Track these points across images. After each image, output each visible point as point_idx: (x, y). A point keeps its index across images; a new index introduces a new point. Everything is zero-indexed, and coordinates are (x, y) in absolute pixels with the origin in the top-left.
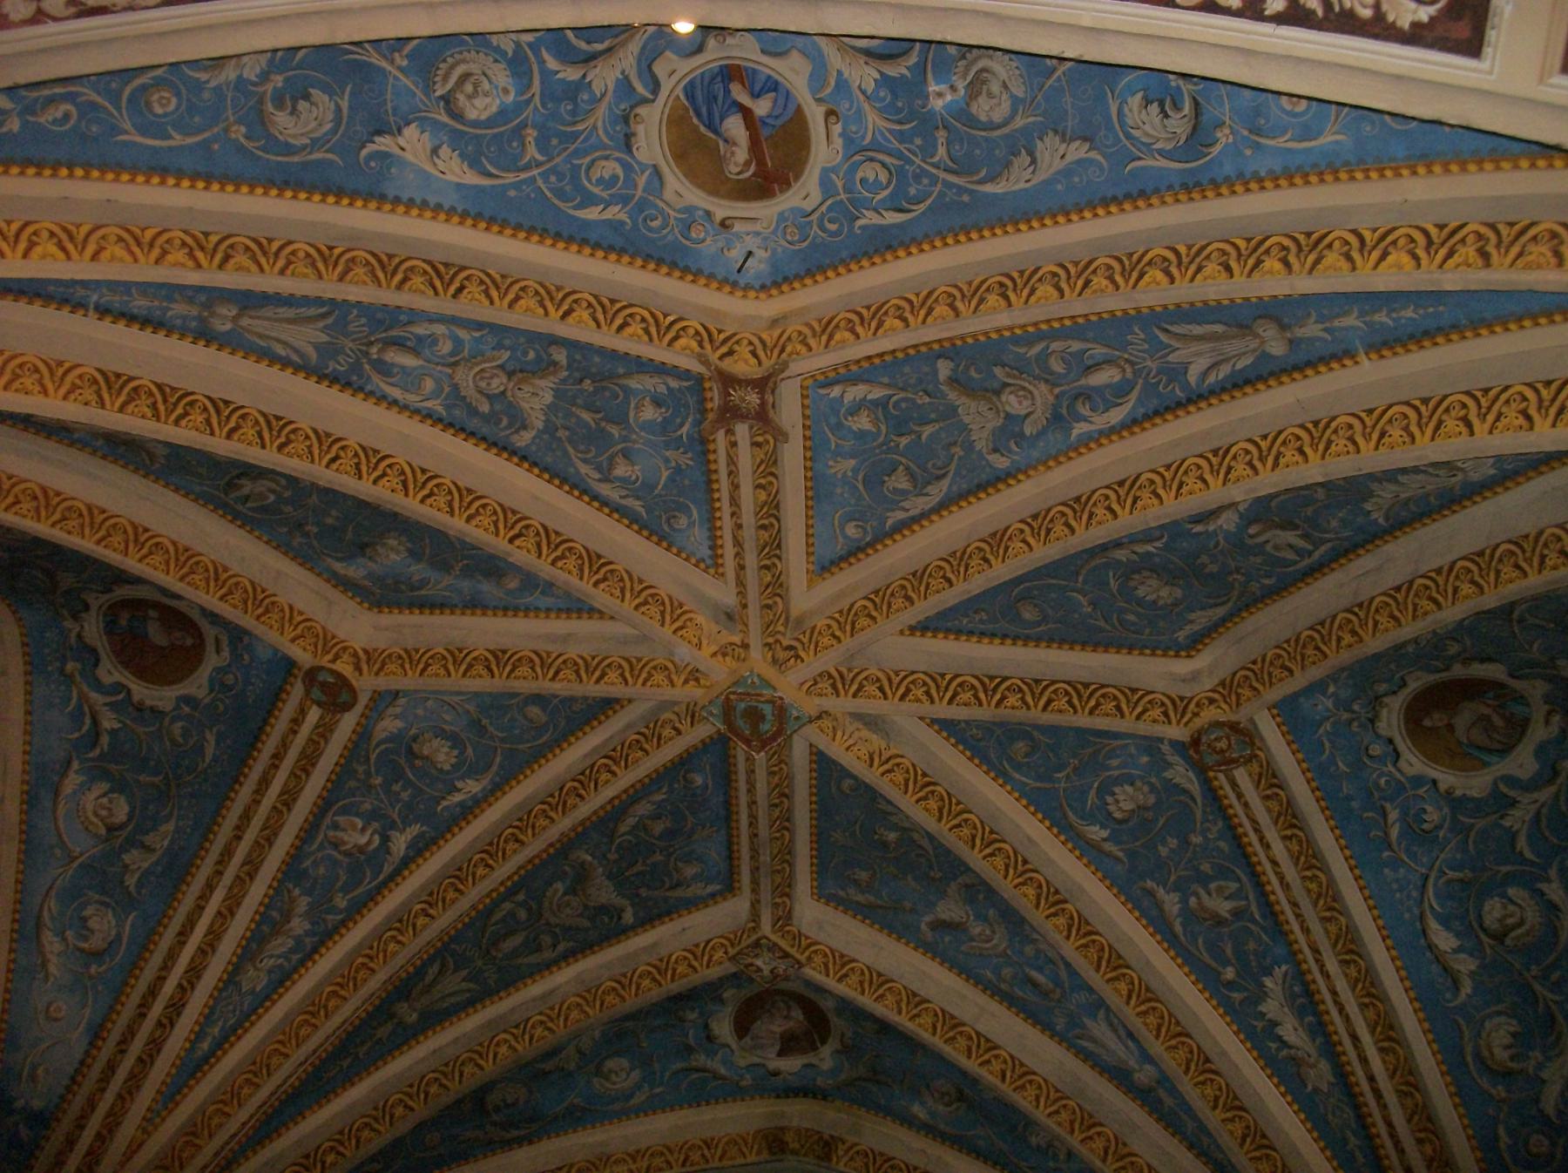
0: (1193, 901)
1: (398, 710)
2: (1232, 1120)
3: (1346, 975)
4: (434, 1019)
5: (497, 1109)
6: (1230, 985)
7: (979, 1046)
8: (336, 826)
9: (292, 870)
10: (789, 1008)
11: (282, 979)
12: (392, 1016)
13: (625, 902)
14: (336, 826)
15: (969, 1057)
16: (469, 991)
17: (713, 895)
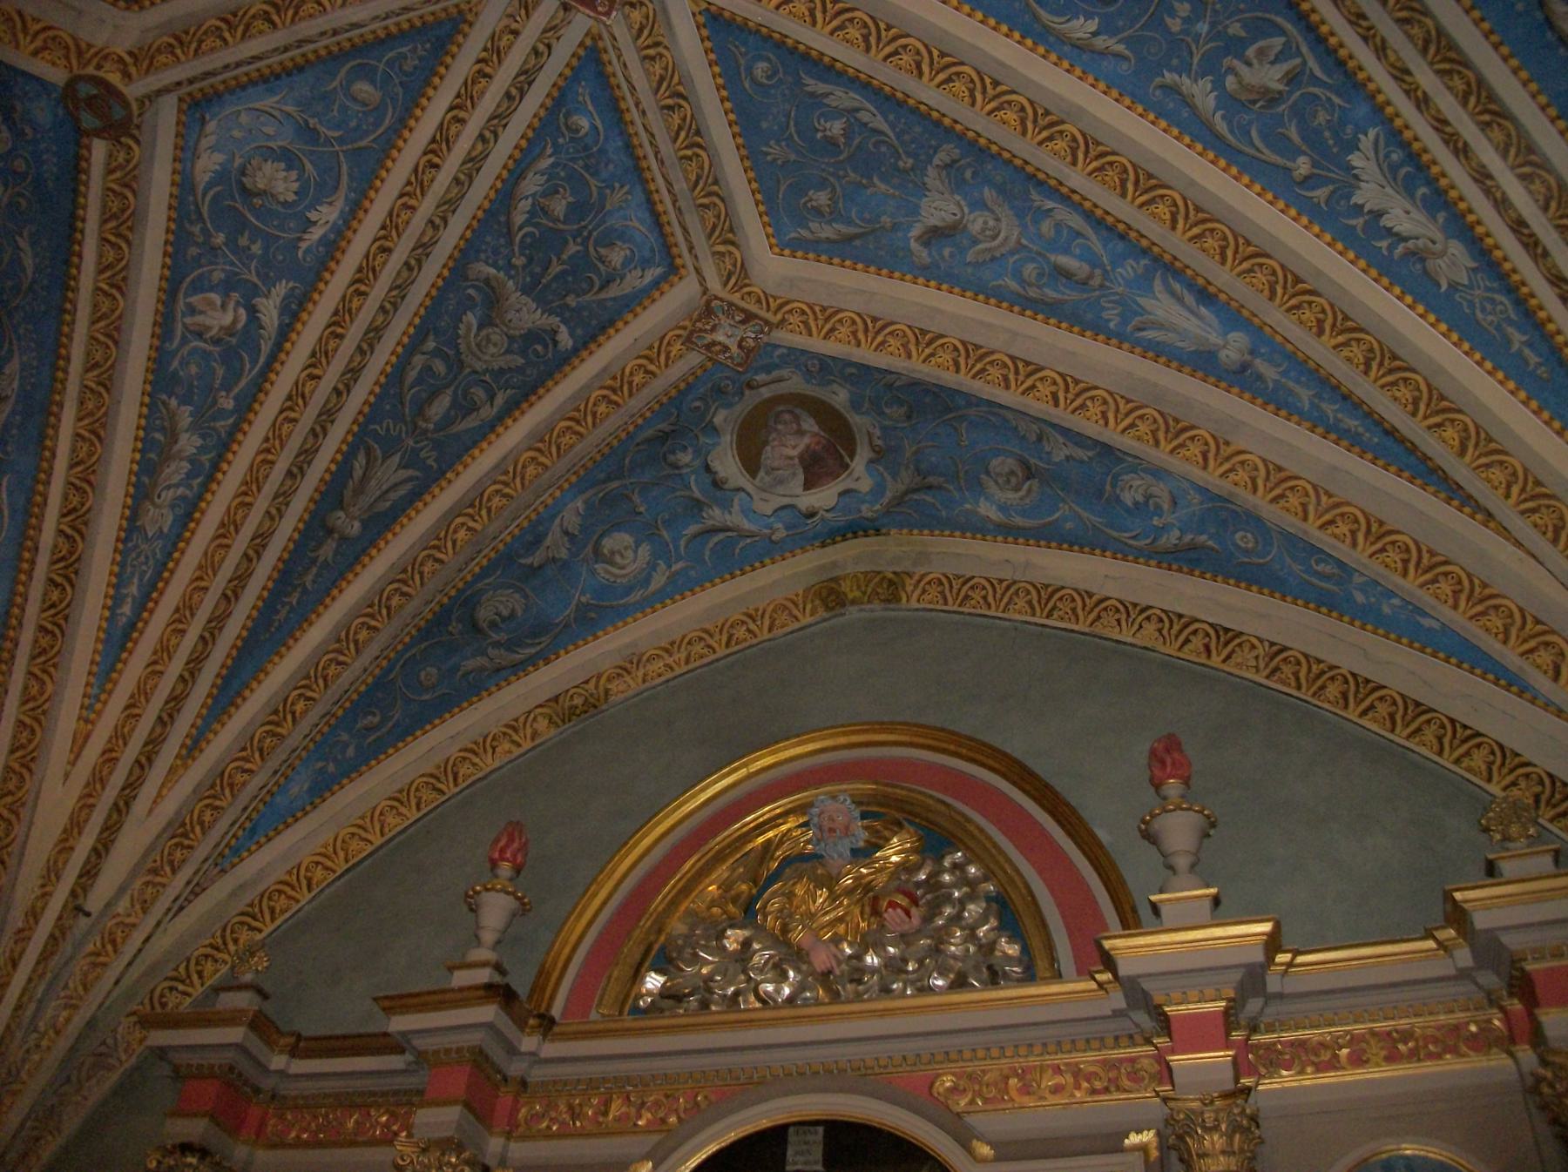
0: (1230, 82)
1: (212, 139)
2: (1346, 344)
3: (1450, 89)
4: (381, 524)
5: (493, 625)
6: (1307, 181)
7: (1017, 372)
8: (192, 310)
9: (161, 378)
10: (797, 418)
11: (189, 513)
12: (330, 531)
13: (554, 320)
14: (192, 310)
15: (1007, 387)
16: (410, 479)
17: (656, 284)
